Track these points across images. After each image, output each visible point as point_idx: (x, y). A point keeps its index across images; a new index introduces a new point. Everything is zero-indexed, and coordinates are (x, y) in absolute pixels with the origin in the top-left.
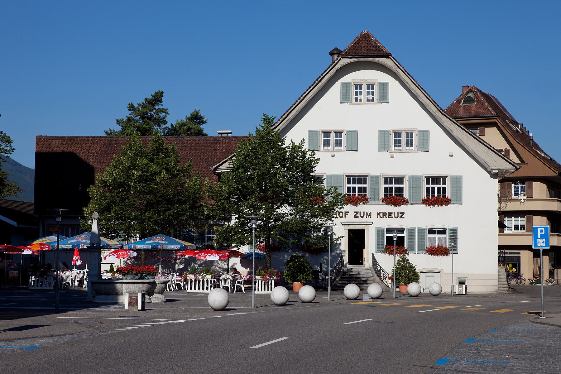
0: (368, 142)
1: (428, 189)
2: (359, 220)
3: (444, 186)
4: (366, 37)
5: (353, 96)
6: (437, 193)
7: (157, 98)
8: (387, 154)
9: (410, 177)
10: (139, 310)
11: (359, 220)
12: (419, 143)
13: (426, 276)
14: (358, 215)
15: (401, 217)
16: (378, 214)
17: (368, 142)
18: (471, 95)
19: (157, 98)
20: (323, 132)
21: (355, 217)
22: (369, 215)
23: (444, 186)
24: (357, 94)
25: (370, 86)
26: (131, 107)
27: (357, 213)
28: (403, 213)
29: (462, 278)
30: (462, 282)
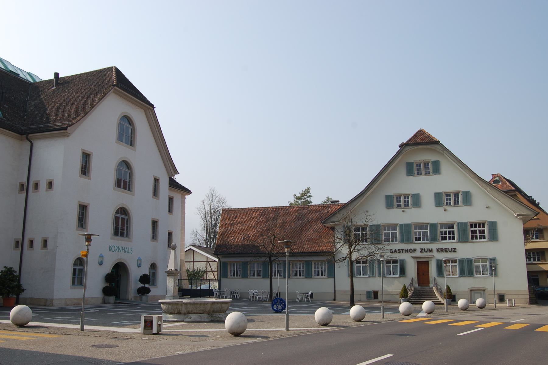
0: (428, 200)
1: (472, 231)
2: (424, 254)
3: (483, 229)
4: (421, 133)
5: (416, 172)
6: (476, 231)
7: (307, 191)
8: (441, 209)
9: (458, 223)
10: (154, 334)
11: (424, 254)
12: (463, 200)
13: (156, 181)
14: (423, 251)
15: (454, 251)
16: (438, 250)
17: (428, 200)
18: (497, 179)
19: (307, 191)
20: (396, 195)
21: (421, 252)
22: (431, 251)
23: (483, 229)
24: (418, 169)
25: (427, 164)
26: (57, 75)
27: (422, 249)
28: (455, 249)
29: (502, 293)
30: (445, 210)
